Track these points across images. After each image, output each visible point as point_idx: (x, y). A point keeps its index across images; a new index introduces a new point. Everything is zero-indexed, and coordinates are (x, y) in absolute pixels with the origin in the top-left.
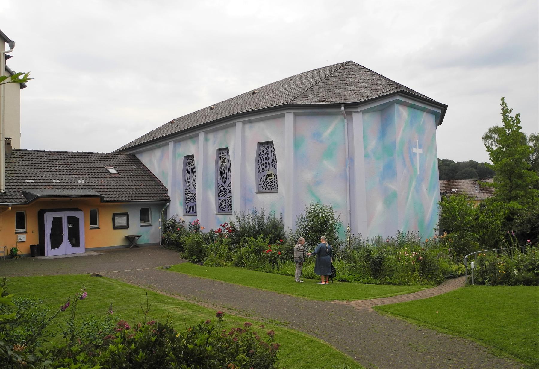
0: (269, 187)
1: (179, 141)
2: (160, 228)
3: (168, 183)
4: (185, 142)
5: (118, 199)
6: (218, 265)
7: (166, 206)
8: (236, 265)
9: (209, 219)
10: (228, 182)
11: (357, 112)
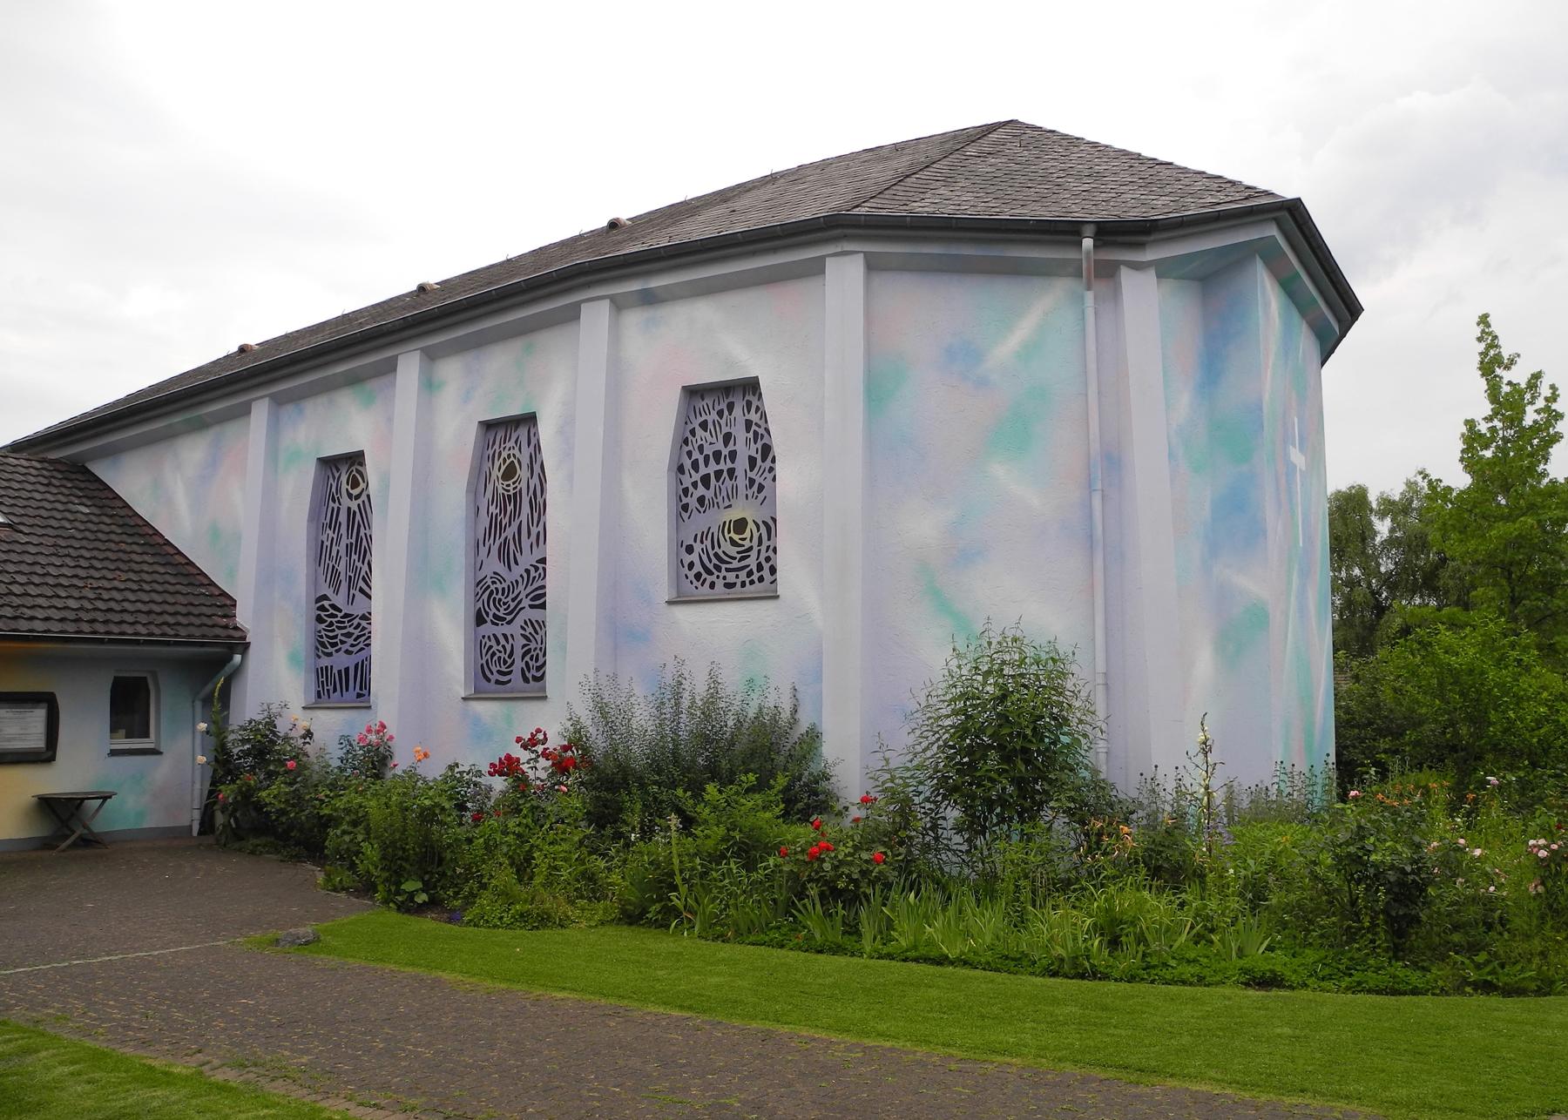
0: (731, 577)
1: (297, 397)
2: (201, 759)
3: (239, 578)
4: (322, 400)
5: (13, 624)
6: (544, 920)
7: (228, 669)
8: (632, 917)
9: (431, 715)
10: (527, 559)
11: (1137, 266)
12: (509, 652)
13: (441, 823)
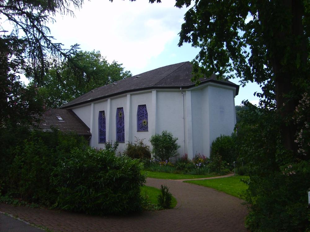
0: (144, 128)
12: (121, 138)
13: (259, 209)
